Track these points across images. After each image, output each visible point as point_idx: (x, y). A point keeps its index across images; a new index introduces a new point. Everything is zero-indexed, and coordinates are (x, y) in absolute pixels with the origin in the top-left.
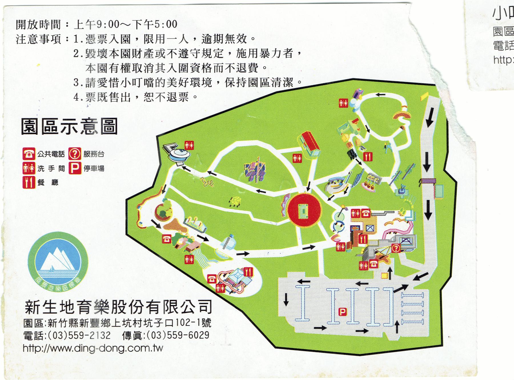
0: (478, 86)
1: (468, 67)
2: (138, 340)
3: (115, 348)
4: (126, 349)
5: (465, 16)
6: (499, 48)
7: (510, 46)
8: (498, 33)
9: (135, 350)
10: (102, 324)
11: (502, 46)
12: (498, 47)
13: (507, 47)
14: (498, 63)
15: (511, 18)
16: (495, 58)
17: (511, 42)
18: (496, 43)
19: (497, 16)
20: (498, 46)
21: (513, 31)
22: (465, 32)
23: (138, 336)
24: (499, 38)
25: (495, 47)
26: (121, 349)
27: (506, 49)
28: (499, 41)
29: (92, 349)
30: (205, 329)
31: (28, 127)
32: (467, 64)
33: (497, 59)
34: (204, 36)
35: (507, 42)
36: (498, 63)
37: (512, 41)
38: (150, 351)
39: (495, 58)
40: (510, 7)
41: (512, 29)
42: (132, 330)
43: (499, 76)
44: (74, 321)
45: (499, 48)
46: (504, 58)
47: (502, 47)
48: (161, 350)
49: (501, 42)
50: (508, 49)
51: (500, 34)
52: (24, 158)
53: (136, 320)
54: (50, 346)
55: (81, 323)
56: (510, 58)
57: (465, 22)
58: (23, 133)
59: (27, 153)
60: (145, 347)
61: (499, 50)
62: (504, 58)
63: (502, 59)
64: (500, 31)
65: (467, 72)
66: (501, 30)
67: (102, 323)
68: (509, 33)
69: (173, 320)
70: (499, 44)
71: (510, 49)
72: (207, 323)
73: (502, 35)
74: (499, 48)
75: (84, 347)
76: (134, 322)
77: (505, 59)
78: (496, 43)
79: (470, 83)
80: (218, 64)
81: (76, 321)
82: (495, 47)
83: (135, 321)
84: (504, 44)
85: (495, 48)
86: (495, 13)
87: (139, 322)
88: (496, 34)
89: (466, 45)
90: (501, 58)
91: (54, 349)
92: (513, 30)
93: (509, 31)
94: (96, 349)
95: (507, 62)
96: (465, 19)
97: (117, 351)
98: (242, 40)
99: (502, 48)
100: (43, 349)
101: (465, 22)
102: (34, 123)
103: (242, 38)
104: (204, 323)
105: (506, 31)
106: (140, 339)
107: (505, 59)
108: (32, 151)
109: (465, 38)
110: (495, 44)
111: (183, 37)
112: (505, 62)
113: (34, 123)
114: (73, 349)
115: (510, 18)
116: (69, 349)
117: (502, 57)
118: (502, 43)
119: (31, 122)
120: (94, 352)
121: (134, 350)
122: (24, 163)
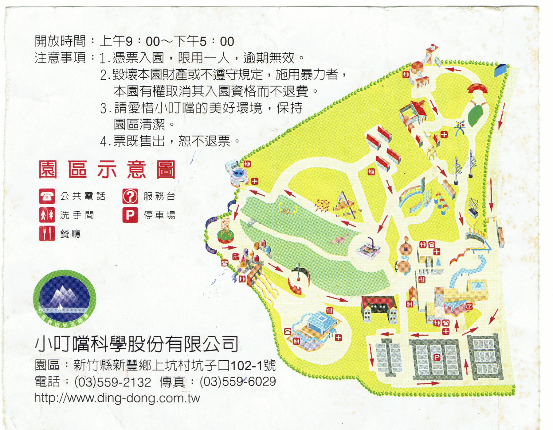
0: (16, 427)
1: (4, 404)
2: (179, 387)
3: (144, 398)
4: (157, 399)
5: (3, 346)
6: (41, 384)
7: (54, 382)
8: (40, 366)
9: (167, 401)
10: (141, 367)
11: (45, 382)
12: (40, 383)
13: (51, 384)
14: (40, 401)
15: (56, 349)
16: (36, 395)
17: (55, 377)
18: (38, 378)
19: (40, 347)
20: (41, 382)
21: (58, 365)
22: (3, 364)
23: (180, 381)
24: (41, 373)
25: (37, 383)
26: (152, 399)
27: (49, 386)
28: (41, 376)
29: (118, 399)
30: (270, 374)
31: (45, 169)
32: (4, 401)
33: (39, 396)
34: (246, 55)
35: (50, 377)
36: (40, 401)
37: (56, 377)
38: (184, 401)
39: (36, 395)
40: (55, 337)
41: (57, 363)
42: (172, 374)
43: (40, 416)
44: (107, 363)
45: (41, 384)
46: (46, 395)
47: (44, 383)
48: (198, 401)
49: (44, 378)
50: (52, 386)
51: (43, 367)
52: (41, 202)
53: (182, 361)
54: (68, 396)
55: (115, 365)
56: (53, 396)
57: (3, 353)
58: (40, 177)
59: (44, 195)
60: (179, 397)
61: (42, 386)
62: (46, 395)
63: (44, 397)
64: (43, 364)
65: (4, 410)
66: (44, 364)
67: (140, 367)
68: (53, 368)
69: (229, 361)
70: (42, 380)
71: (54, 386)
72: (270, 365)
73: (45, 369)
74: (41, 383)
75: (109, 397)
76: (180, 363)
77: (48, 397)
78: (38, 378)
79: (6, 423)
80: (263, 86)
81: (109, 363)
82: (37, 383)
83: (181, 362)
84: (48, 379)
85: (37, 384)
86: (38, 344)
87: (187, 364)
88: (38, 368)
89: (3, 379)
90: (43, 395)
91: (72, 399)
92: (58, 363)
93: (53, 365)
94: (123, 399)
95: (50, 400)
96: (3, 349)
97: (147, 402)
98: (289, 60)
99: (44, 384)
100: (58, 399)
101: (3, 353)
102: (53, 166)
103: (289, 56)
104: (266, 365)
105: (50, 364)
106: (183, 386)
107: (48, 397)
108: (52, 194)
109: (3, 371)
110: (36, 379)
111: (224, 56)
112: (48, 400)
113: (53, 166)
114: (95, 399)
115: (55, 350)
116: (90, 399)
117: (44, 394)
118: (45, 379)
119: (49, 165)
120: (120, 402)
121: (166, 401)
122: (41, 209)
